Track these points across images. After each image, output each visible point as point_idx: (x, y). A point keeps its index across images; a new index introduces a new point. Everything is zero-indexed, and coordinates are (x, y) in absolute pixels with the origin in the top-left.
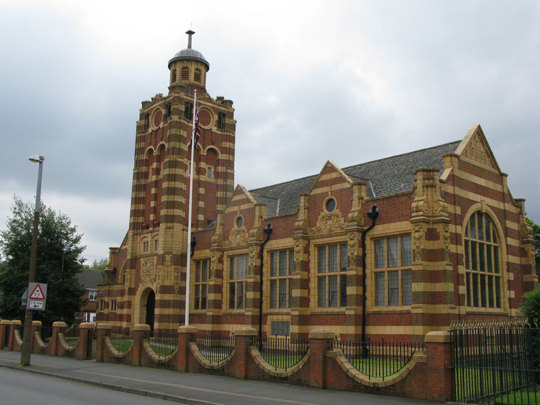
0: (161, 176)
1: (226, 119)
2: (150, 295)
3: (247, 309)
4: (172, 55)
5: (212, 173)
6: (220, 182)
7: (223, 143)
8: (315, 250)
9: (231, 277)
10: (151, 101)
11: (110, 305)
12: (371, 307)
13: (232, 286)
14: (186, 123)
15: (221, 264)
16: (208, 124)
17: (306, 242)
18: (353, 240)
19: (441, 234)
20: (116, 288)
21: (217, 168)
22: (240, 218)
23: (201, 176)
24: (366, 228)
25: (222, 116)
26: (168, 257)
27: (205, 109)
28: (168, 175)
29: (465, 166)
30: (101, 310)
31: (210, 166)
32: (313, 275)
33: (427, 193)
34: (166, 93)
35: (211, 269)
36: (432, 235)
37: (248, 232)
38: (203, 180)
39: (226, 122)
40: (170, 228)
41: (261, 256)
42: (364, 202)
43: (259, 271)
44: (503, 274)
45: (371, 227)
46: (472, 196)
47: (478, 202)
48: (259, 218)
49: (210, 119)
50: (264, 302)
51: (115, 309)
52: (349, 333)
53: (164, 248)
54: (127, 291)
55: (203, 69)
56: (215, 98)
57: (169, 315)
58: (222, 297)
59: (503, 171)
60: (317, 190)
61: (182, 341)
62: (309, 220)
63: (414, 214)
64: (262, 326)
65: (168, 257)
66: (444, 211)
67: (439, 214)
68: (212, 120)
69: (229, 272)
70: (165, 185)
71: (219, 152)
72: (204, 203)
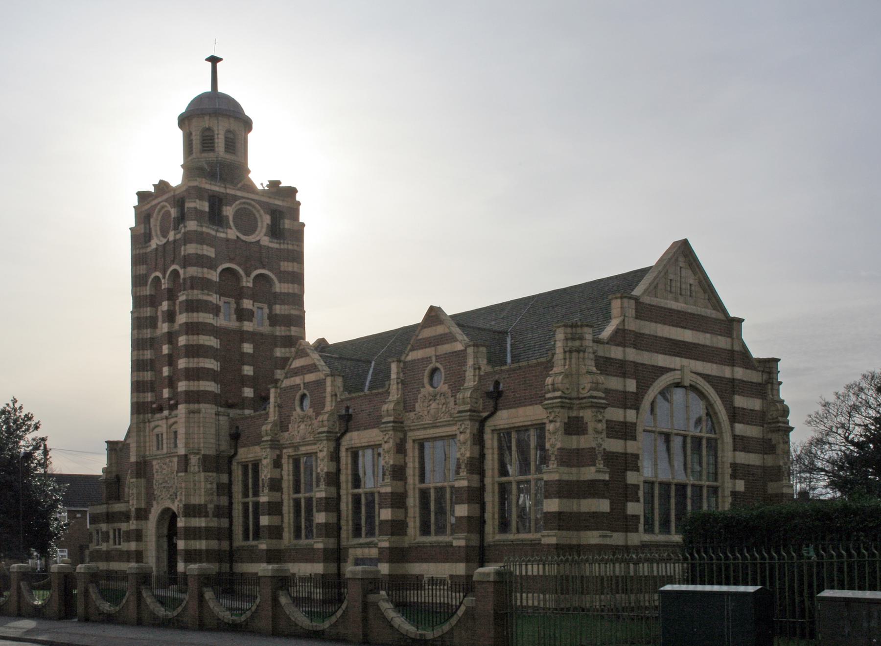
0: (176, 326)
2: (169, 517)
3: (456, 536)
5: (266, 316)
6: (280, 331)
7: (282, 263)
8: (414, 448)
9: (422, 479)
10: (152, 189)
11: (112, 536)
12: (492, 534)
13: (424, 495)
14: (213, 233)
15: (279, 470)
16: (251, 234)
17: (400, 435)
18: (465, 432)
19: (589, 424)
20: (118, 507)
22: (435, 370)
23: (246, 323)
24: (485, 414)
26: (194, 460)
28: (186, 324)
29: (644, 311)
30: (98, 544)
31: (260, 305)
32: (412, 487)
33: (570, 361)
34: (176, 178)
35: (319, 470)
36: (574, 427)
37: (454, 396)
38: (251, 329)
40: (193, 412)
41: (479, 439)
42: (482, 373)
43: (477, 466)
44: (723, 482)
45: (492, 414)
46: (662, 360)
47: (675, 370)
48: (332, 396)
49: (255, 218)
50: (344, 528)
51: (120, 544)
52: (458, 573)
53: (187, 445)
54: (133, 514)
57: (200, 551)
58: (282, 521)
59: (732, 314)
60: (415, 352)
61: (193, 585)
62: (405, 402)
63: (548, 395)
64: (342, 564)
65: (194, 460)
66: (596, 389)
67: (588, 394)
68: (259, 224)
69: (291, 483)
70: (182, 340)
72: (252, 368)
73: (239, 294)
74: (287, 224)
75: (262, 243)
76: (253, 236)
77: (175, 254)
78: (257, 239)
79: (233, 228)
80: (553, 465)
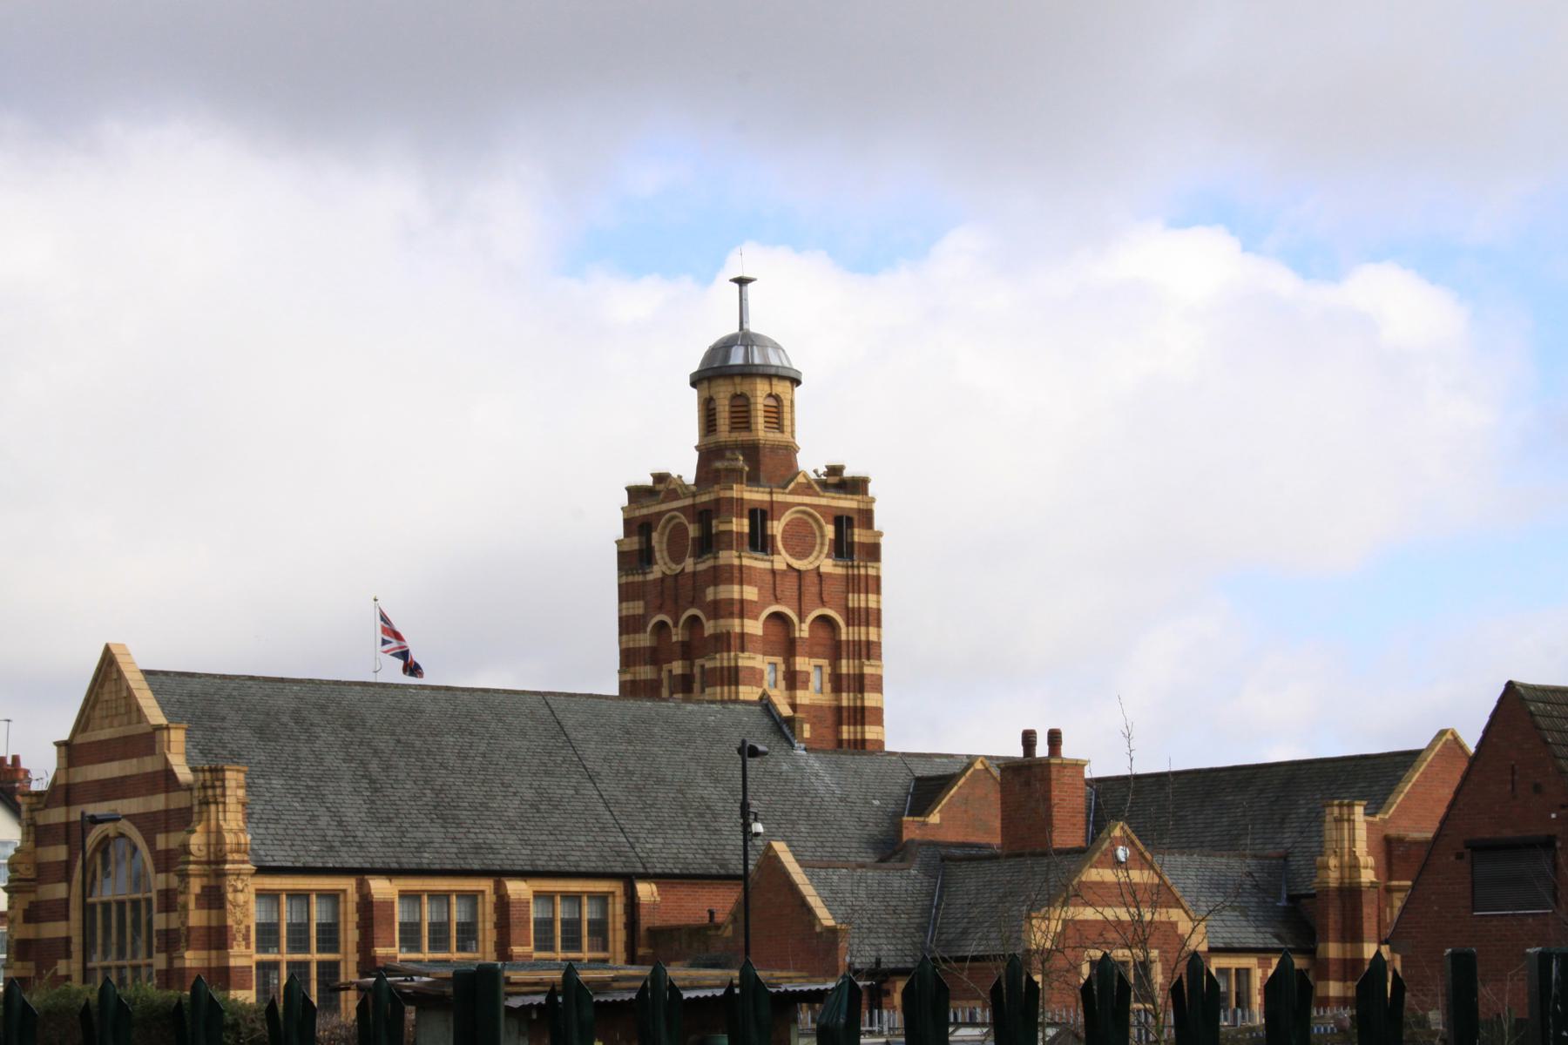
1: (856, 531)
6: (846, 700)
34: (685, 468)
39: (856, 539)
49: (813, 547)
71: (842, 623)
74: (859, 535)
75: (822, 570)
79: (783, 551)
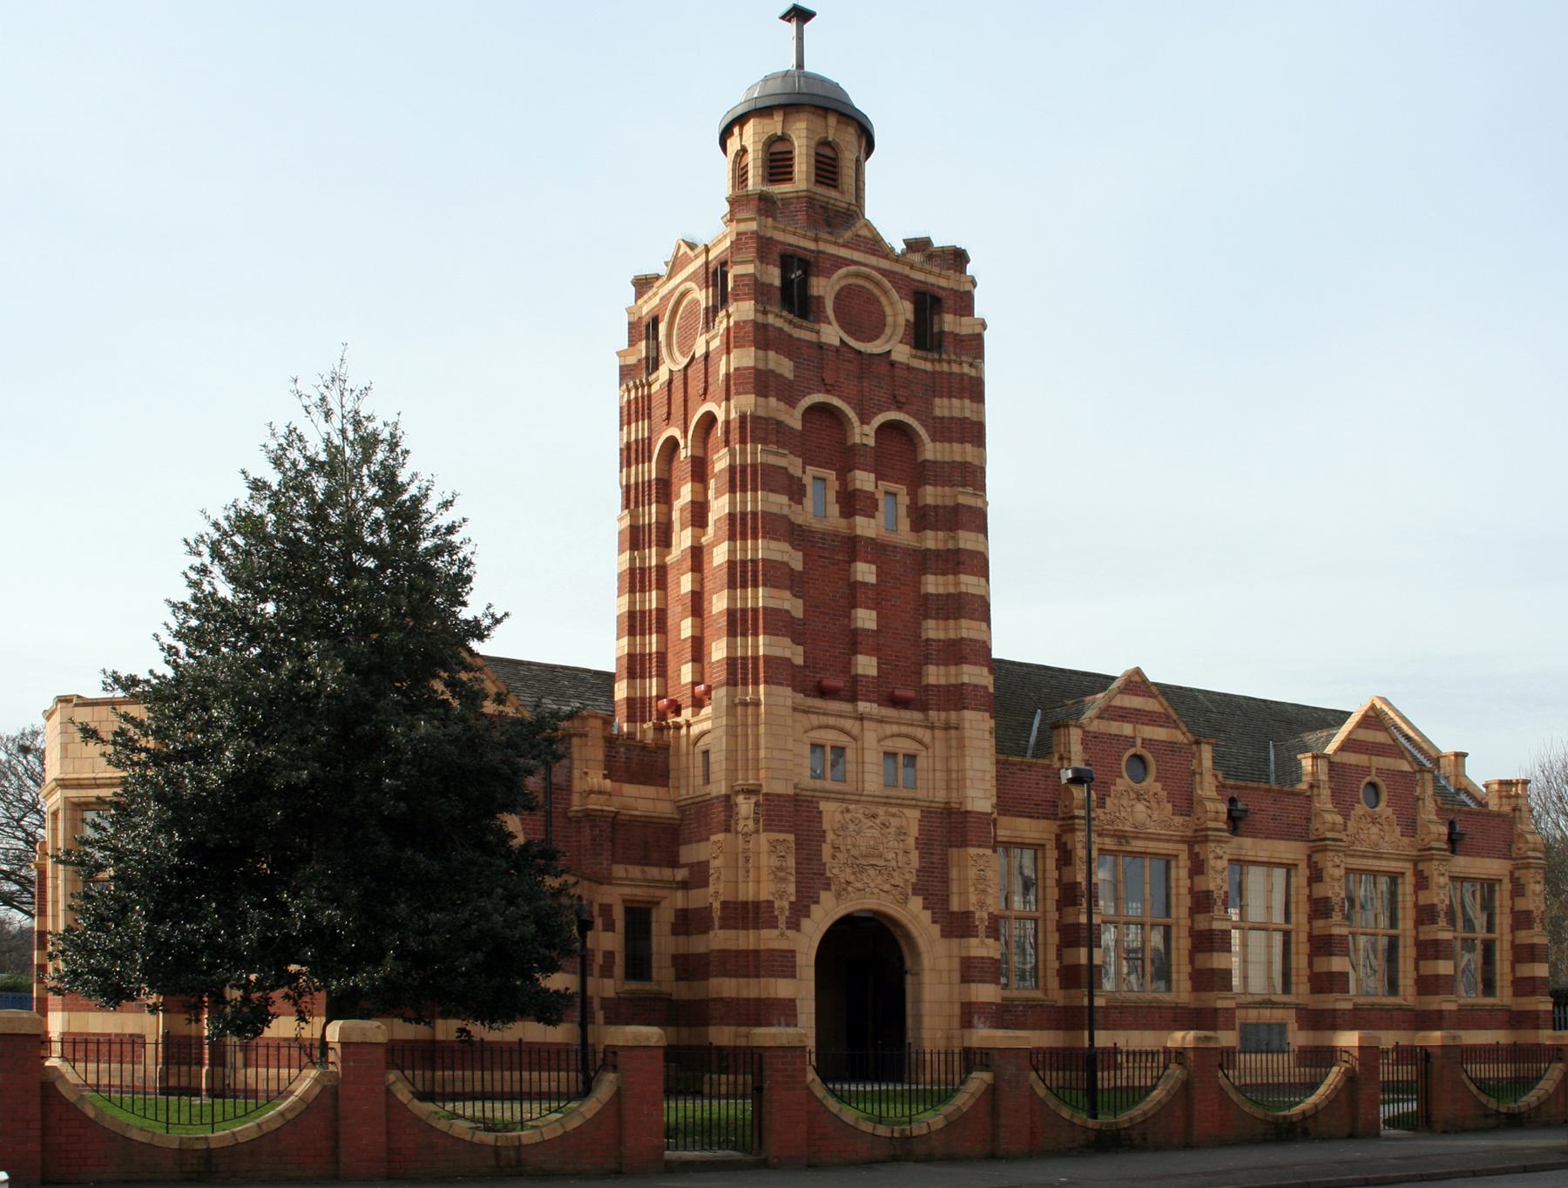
4: (735, 98)
5: (902, 511)
6: (932, 540)
7: (937, 401)
21: (920, 491)
23: (859, 520)
25: (928, 304)
27: (861, 282)
31: (893, 487)
38: (871, 533)
55: (848, 141)
56: (899, 247)
65: (745, 806)
73: (845, 459)
76: (877, 342)
77: (706, 382)
78: (886, 348)
80: (1442, 907)
